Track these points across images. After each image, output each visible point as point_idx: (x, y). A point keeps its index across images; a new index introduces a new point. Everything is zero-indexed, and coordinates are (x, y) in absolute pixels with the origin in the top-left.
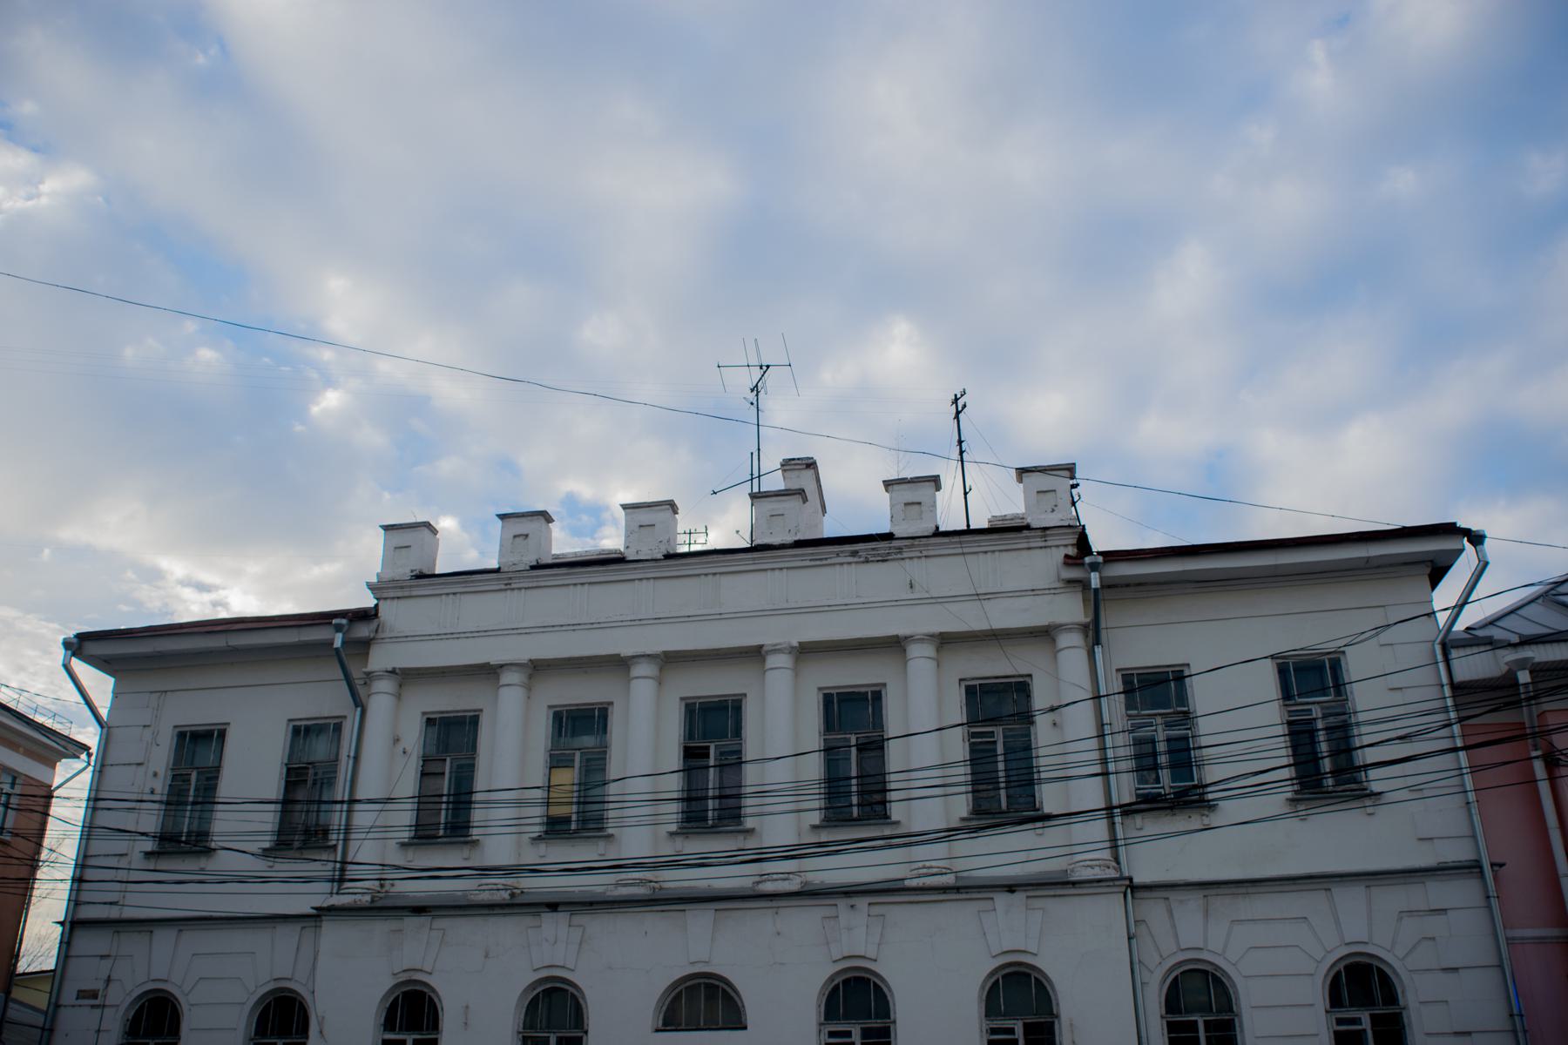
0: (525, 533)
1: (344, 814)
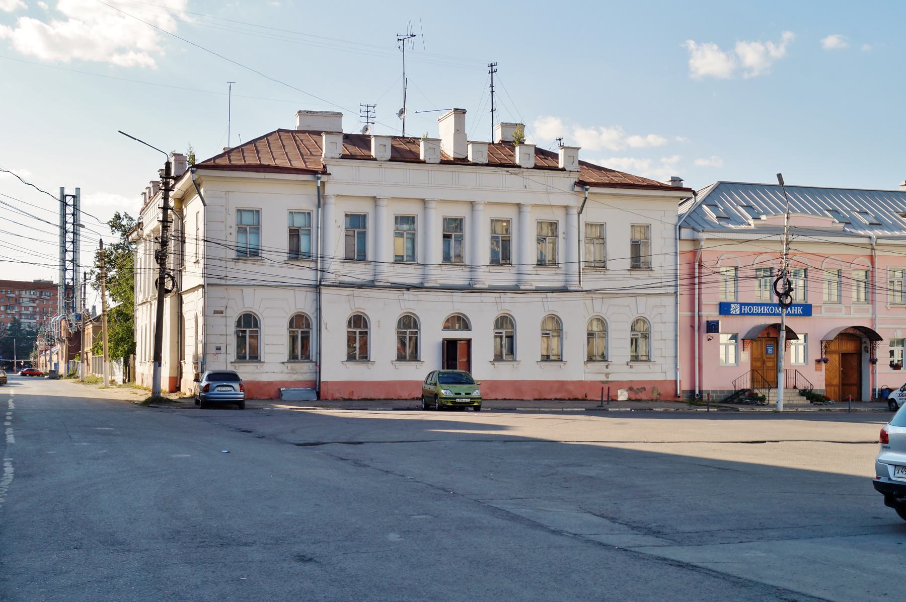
0: (384, 144)
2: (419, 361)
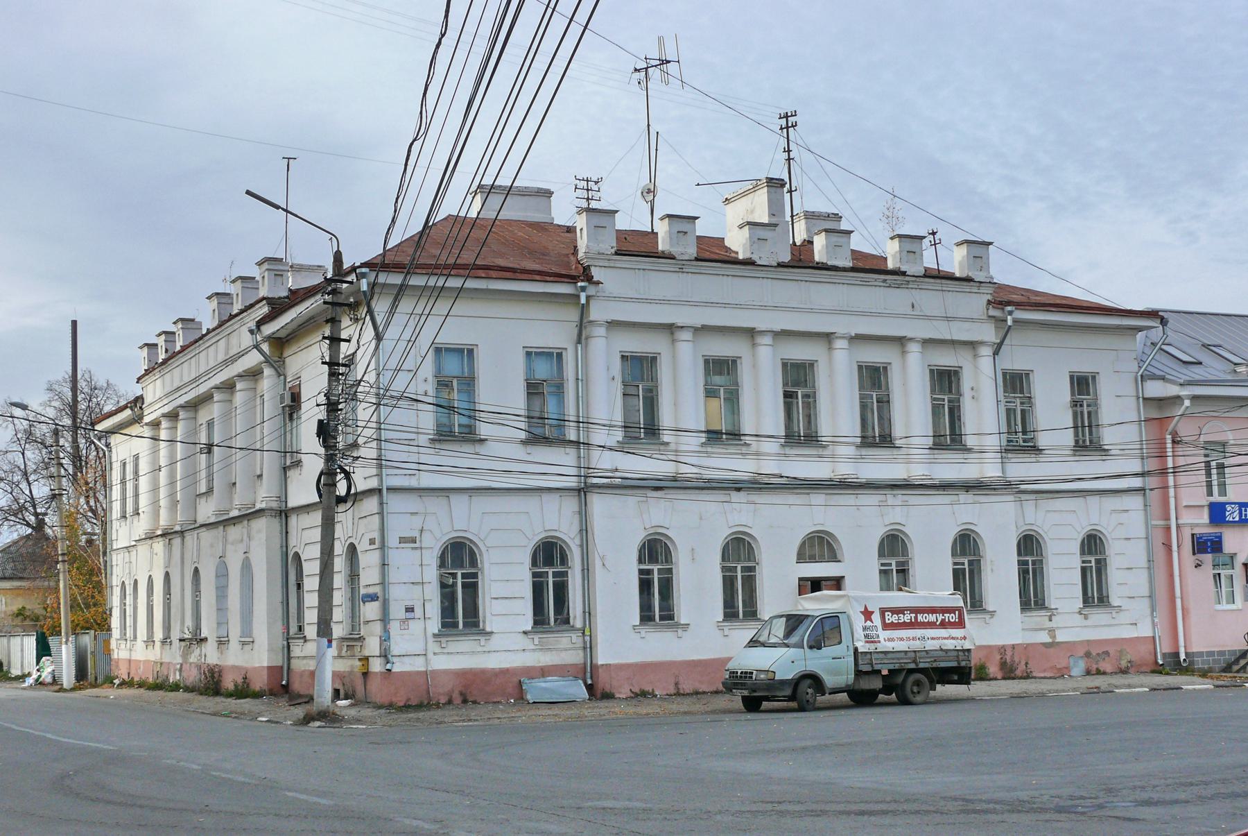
1: (581, 415)
2: (985, 611)
